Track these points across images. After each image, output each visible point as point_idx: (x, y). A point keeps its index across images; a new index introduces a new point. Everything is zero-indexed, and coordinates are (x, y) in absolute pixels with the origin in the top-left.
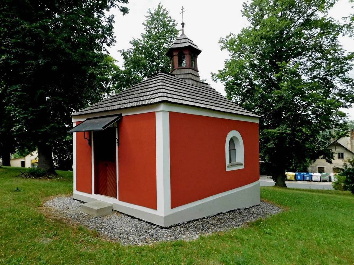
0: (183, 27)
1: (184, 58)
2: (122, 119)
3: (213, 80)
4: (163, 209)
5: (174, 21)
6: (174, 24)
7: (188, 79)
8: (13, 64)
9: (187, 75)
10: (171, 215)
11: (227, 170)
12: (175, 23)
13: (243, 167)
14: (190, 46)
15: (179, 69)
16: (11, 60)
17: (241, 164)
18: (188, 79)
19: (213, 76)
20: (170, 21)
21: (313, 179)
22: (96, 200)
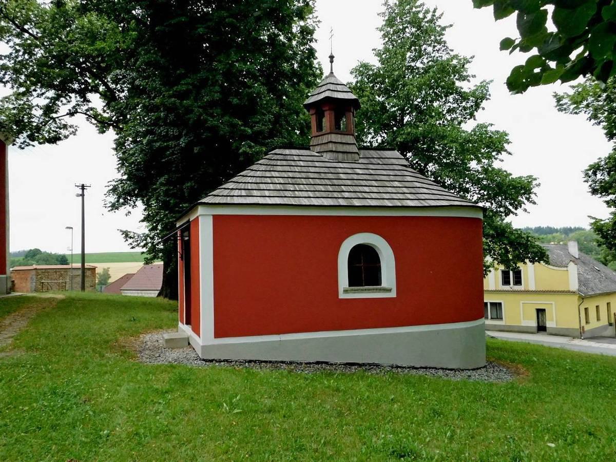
0: (332, 62)
1: (324, 116)
2: (190, 224)
3: (560, 110)
4: (204, 337)
5: (435, 11)
6: (434, 15)
7: (327, 152)
8: (157, 148)
9: (326, 145)
10: (214, 346)
11: (342, 296)
12: (437, 14)
13: (393, 294)
14: (327, 99)
15: (317, 136)
16: (156, 141)
17: (389, 290)
18: (327, 152)
19: (559, 100)
20: (427, 12)
21: (549, 324)
22: (185, 332)
